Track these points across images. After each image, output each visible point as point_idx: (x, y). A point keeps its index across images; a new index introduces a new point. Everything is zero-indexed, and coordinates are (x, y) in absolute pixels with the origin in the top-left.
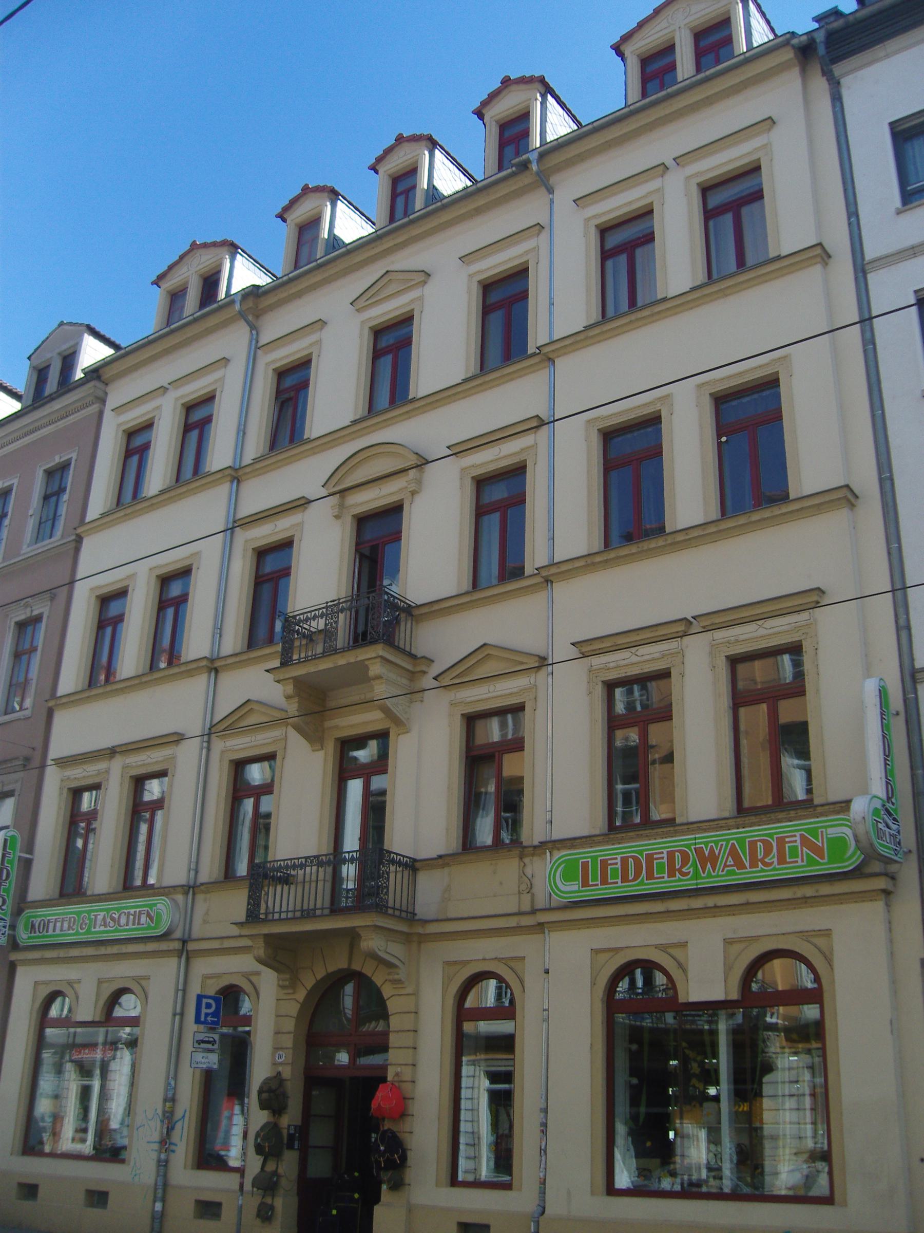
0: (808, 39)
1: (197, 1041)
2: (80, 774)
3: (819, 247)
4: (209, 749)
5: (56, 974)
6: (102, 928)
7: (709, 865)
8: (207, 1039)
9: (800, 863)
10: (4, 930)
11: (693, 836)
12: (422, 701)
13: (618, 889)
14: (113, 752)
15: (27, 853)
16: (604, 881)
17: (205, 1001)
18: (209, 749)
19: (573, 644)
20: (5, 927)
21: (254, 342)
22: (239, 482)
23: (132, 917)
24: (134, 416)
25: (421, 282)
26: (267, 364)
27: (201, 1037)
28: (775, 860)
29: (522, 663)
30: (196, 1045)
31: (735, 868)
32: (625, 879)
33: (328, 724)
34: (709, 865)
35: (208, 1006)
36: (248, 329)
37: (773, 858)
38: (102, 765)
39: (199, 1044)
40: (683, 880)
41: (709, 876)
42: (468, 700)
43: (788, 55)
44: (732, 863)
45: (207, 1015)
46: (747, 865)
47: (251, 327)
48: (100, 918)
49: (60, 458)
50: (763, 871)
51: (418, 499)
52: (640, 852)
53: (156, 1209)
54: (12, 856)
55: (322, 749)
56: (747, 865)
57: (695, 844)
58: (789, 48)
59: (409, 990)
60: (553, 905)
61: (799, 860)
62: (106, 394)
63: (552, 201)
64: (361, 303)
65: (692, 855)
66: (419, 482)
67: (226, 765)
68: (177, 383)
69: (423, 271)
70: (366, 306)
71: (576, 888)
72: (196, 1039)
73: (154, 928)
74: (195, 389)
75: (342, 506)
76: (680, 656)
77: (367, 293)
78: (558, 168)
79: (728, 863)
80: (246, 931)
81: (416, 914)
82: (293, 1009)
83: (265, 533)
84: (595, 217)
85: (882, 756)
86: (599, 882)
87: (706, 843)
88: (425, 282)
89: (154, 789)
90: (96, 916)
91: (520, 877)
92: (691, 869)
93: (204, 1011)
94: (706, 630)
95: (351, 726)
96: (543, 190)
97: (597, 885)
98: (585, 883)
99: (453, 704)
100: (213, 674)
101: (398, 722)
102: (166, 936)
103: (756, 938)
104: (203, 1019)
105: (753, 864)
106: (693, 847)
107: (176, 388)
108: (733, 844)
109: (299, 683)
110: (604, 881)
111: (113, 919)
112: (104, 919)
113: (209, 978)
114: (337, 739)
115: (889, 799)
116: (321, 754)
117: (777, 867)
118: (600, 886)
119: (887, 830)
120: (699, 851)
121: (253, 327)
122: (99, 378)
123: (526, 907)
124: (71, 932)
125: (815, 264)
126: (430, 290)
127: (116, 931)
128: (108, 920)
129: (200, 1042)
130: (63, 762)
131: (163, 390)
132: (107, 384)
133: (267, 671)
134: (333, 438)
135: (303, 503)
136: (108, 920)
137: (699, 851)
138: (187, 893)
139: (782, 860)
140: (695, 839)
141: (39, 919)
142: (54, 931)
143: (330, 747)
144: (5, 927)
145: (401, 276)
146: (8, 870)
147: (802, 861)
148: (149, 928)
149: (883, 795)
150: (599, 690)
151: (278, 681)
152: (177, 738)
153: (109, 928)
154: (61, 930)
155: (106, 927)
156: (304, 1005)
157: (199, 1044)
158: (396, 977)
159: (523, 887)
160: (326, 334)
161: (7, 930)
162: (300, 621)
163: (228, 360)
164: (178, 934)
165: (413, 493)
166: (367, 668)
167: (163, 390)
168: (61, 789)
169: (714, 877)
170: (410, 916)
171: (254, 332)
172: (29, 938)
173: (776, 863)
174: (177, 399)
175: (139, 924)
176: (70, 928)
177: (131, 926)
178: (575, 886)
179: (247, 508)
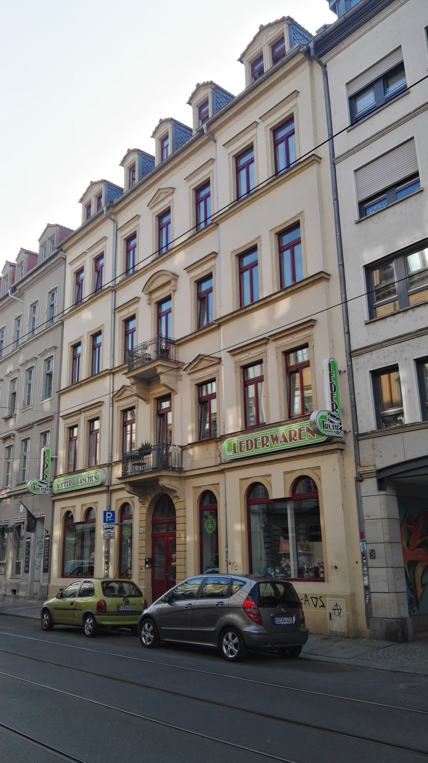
0: (307, 47)
1: (105, 529)
2: (71, 421)
3: (314, 156)
4: (113, 407)
5: (67, 504)
6: (81, 484)
7: (275, 442)
8: (109, 527)
9: (306, 439)
10: (47, 488)
11: (270, 430)
12: (181, 380)
13: (246, 454)
14: (80, 411)
15: (56, 456)
16: (241, 451)
17: (107, 513)
18: (113, 407)
19: (5, 376)
20: (48, 487)
21: (115, 227)
22: (115, 292)
23: (90, 478)
24: (77, 266)
25: (171, 193)
26: (122, 237)
27: (106, 527)
28: (298, 438)
29: (213, 361)
30: (105, 530)
31: (284, 442)
32: (248, 449)
33: (151, 393)
34: (275, 442)
35: (109, 515)
36: (112, 222)
37: (297, 437)
38: (77, 417)
39: (106, 530)
40: (267, 449)
41: (276, 446)
42: (197, 378)
43: (300, 57)
44: (283, 440)
45: (108, 519)
46: (288, 441)
47: (113, 221)
48: (79, 480)
49: (53, 287)
50: (294, 443)
51: (176, 293)
52: (252, 438)
53: (148, 565)
54: (48, 458)
55: (149, 403)
56: (288, 441)
57: (271, 433)
58: (300, 54)
59: (182, 500)
60: (226, 462)
61: (306, 437)
62: (66, 256)
63: (216, 145)
64: (151, 205)
65: (270, 438)
66: (176, 286)
67: (119, 412)
68: (90, 249)
69: (171, 188)
70: (154, 206)
71: (231, 454)
72: (104, 528)
73: (97, 482)
74: (96, 252)
75: (150, 299)
76: (266, 353)
77: (153, 200)
78: (217, 130)
79: (282, 440)
80: (122, 481)
81: (183, 468)
82: (145, 510)
83: (126, 314)
84: (232, 152)
85: (330, 392)
86: (239, 451)
87: (274, 432)
88: (173, 192)
89: (97, 425)
90: (78, 479)
91: (216, 451)
92: (269, 444)
93: (107, 517)
94: (274, 340)
95: (158, 393)
96: (212, 142)
97: (238, 452)
98: (235, 452)
99: (192, 380)
100: (112, 375)
101: (173, 391)
102: (101, 485)
103: (292, 471)
104: (107, 521)
105: (291, 441)
106: (270, 434)
107: (90, 252)
108: (283, 432)
109: (134, 377)
110: (241, 451)
111: (83, 480)
112: (81, 480)
113: (119, 500)
114: (155, 398)
115: (333, 410)
116: (149, 405)
117: (299, 441)
118: (239, 453)
119: (331, 424)
120: (272, 436)
121: (114, 221)
122: (62, 250)
123: (218, 462)
124: (70, 486)
125: (314, 164)
126: (175, 196)
127: (85, 484)
128: (82, 480)
129: (106, 529)
130: (65, 417)
131: (85, 253)
132: (65, 252)
133: (123, 374)
134: (146, 269)
135: (136, 300)
136: (82, 480)
137: (272, 436)
138: (108, 466)
139: (300, 438)
140: (270, 431)
141: (60, 482)
142: (65, 487)
143: (152, 402)
144: (48, 487)
145: (164, 191)
146: (46, 464)
147: (307, 438)
148: (96, 482)
149: (329, 408)
150: (239, 370)
151: (128, 378)
152: (100, 404)
153: (82, 484)
154: (67, 486)
155: (81, 483)
156: (148, 509)
157: (106, 530)
158: (176, 495)
159: (217, 454)
160: (141, 221)
161: (49, 488)
162: (138, 350)
163: (107, 237)
164: (106, 484)
165: (174, 291)
166: (156, 370)
167: (85, 253)
168: (65, 428)
169: (277, 446)
170: (181, 470)
171: (115, 223)
172: (57, 490)
173: (298, 439)
174: (91, 256)
175: (92, 481)
176: (70, 485)
177: (90, 482)
178: (231, 453)
179: (119, 303)
